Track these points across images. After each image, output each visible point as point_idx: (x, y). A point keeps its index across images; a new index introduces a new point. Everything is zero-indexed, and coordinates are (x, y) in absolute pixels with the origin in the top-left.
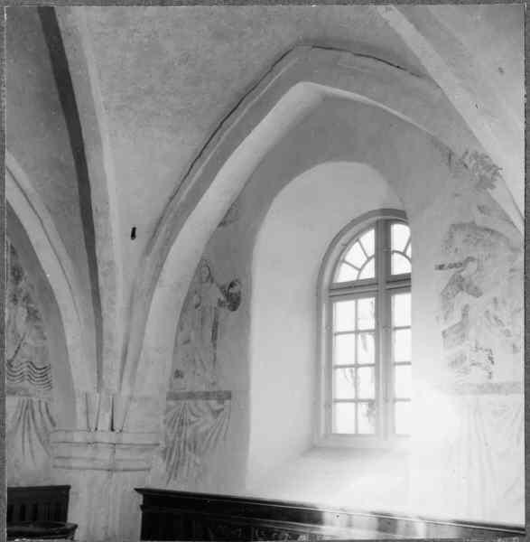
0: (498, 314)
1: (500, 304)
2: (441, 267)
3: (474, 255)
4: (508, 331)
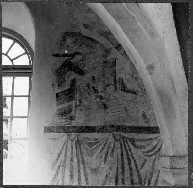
0: (95, 86)
1: (97, 81)
2: (57, 55)
3: (80, 51)
4: (101, 96)
